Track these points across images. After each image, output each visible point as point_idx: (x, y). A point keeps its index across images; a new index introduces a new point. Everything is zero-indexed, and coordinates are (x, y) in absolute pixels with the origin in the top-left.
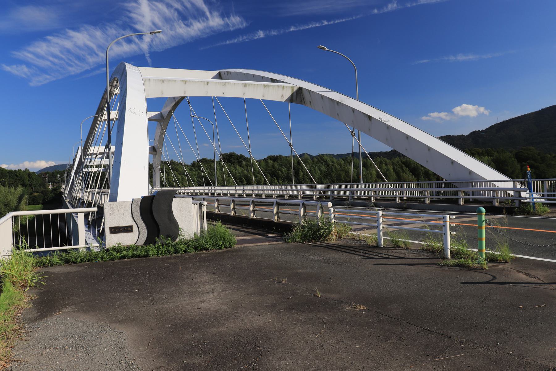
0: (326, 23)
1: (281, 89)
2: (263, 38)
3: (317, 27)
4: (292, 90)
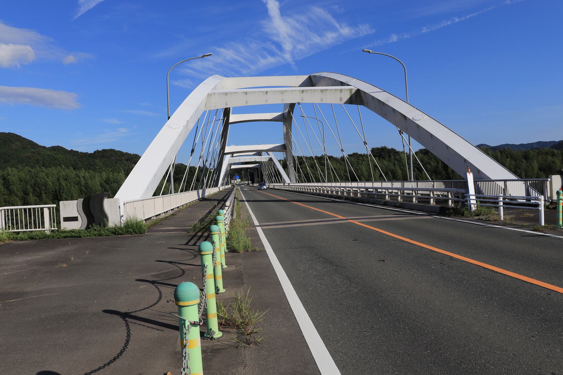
1: (339, 92)
4: (351, 92)
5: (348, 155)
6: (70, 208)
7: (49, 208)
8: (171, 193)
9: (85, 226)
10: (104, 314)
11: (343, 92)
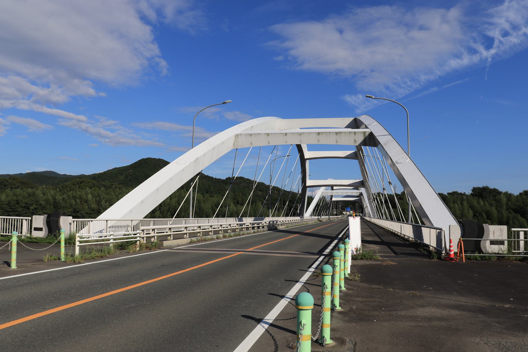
1: (353, 134)
4: (364, 135)
5: (448, 194)
6: (39, 221)
7: (26, 220)
8: (188, 217)
9: (47, 235)
10: (242, 318)
11: (357, 135)
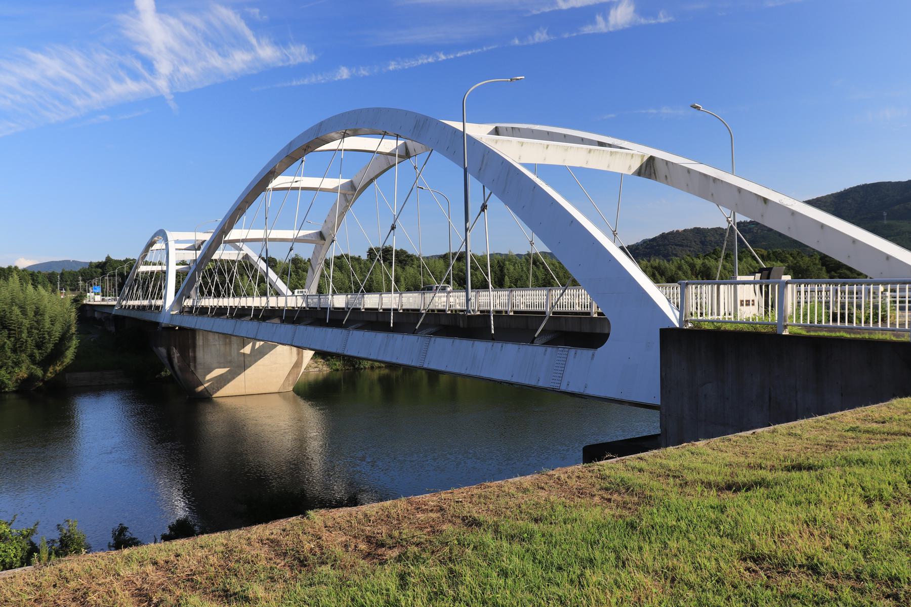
0: (442, 57)
1: (630, 157)
2: (346, 80)
3: (429, 64)
